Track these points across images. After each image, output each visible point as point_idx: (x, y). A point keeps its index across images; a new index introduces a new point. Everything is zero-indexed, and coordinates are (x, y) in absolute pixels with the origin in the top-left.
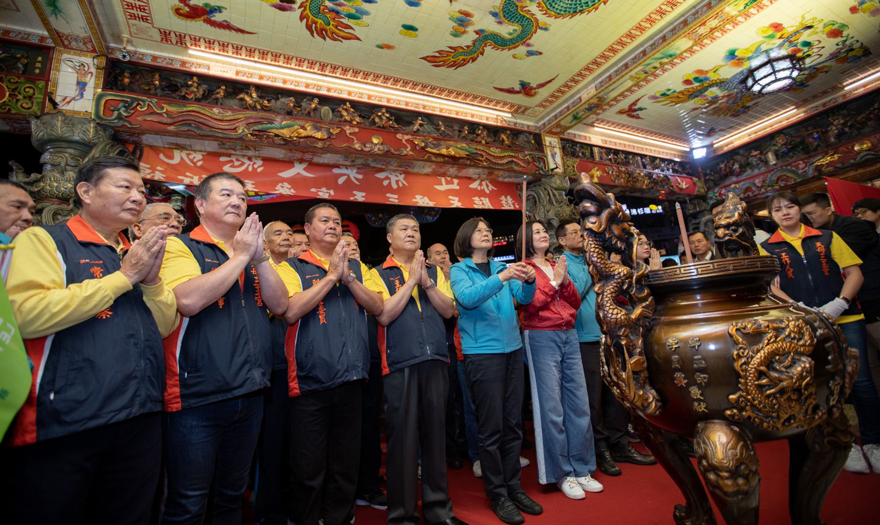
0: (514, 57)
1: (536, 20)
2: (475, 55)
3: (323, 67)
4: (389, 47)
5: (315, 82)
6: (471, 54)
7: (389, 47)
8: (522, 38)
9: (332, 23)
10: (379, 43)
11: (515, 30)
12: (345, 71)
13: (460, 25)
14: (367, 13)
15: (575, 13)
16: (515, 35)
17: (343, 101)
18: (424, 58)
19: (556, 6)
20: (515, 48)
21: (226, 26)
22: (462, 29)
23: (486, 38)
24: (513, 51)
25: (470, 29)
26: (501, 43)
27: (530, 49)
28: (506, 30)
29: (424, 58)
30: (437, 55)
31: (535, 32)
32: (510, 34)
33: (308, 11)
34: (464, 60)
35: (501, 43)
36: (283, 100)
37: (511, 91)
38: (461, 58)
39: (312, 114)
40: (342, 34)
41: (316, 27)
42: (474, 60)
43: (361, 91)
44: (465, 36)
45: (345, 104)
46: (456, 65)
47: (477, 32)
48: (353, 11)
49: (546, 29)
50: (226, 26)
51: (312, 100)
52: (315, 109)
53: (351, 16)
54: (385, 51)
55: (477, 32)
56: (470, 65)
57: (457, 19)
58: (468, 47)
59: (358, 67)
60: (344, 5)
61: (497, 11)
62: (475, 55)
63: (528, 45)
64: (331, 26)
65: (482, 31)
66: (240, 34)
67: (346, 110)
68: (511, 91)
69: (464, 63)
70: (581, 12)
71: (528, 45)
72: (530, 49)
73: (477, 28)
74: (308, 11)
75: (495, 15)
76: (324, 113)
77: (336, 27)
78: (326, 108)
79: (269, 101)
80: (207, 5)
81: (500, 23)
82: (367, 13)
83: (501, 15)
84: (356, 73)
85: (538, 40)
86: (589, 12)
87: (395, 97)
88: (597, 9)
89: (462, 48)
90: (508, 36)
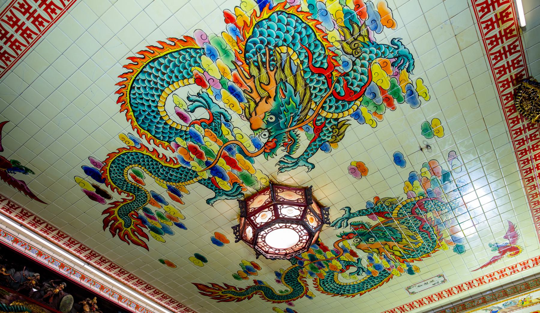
0: (274, 309)
1: (307, 289)
2: (243, 297)
3: (92, 255)
4: (170, 265)
5: (72, 265)
6: (241, 295)
7: (170, 265)
8: (288, 298)
9: (132, 227)
10: (164, 258)
11: (287, 291)
12: (112, 267)
13: (245, 272)
14: (171, 233)
15: (338, 294)
16: (285, 294)
17: (91, 294)
18: (196, 284)
19: (327, 285)
20: (279, 303)
21: (21, 186)
22: (245, 275)
23: (260, 288)
24: (276, 305)
25: (252, 278)
26: (269, 294)
27: (290, 307)
28: (279, 288)
29: (196, 284)
30: (210, 286)
31: (301, 297)
32: (281, 292)
33: (116, 210)
34: (231, 297)
35: (269, 294)
36: (26, 273)
37: (494, 260)
38: (229, 295)
39: (51, 300)
40: (134, 238)
41: (113, 224)
42: (239, 300)
43: (114, 289)
44: (244, 281)
45: (92, 299)
46: (221, 299)
47: (255, 282)
48: (159, 227)
49: (310, 298)
50: (21, 186)
51: (58, 284)
52: (58, 294)
53: (154, 230)
54: (165, 266)
55: (255, 282)
56: (233, 303)
57: (246, 267)
58: (241, 289)
59: (125, 267)
60: (155, 219)
61: (282, 273)
62: (243, 297)
63: (291, 304)
64: (129, 229)
65: (260, 282)
66: (28, 198)
67: (90, 305)
68: (494, 260)
69: (230, 299)
70: (342, 295)
71: (291, 304)
72: (290, 307)
73: (258, 278)
74: (116, 210)
75: (278, 274)
76: (65, 303)
77: (133, 232)
78: (70, 296)
79: (8, 269)
80: (15, 162)
81: (278, 282)
82: (171, 233)
83: (283, 276)
84: (122, 272)
85: (300, 304)
86: (347, 297)
87: (144, 305)
88: (353, 296)
89: (235, 288)
90: (278, 293)
